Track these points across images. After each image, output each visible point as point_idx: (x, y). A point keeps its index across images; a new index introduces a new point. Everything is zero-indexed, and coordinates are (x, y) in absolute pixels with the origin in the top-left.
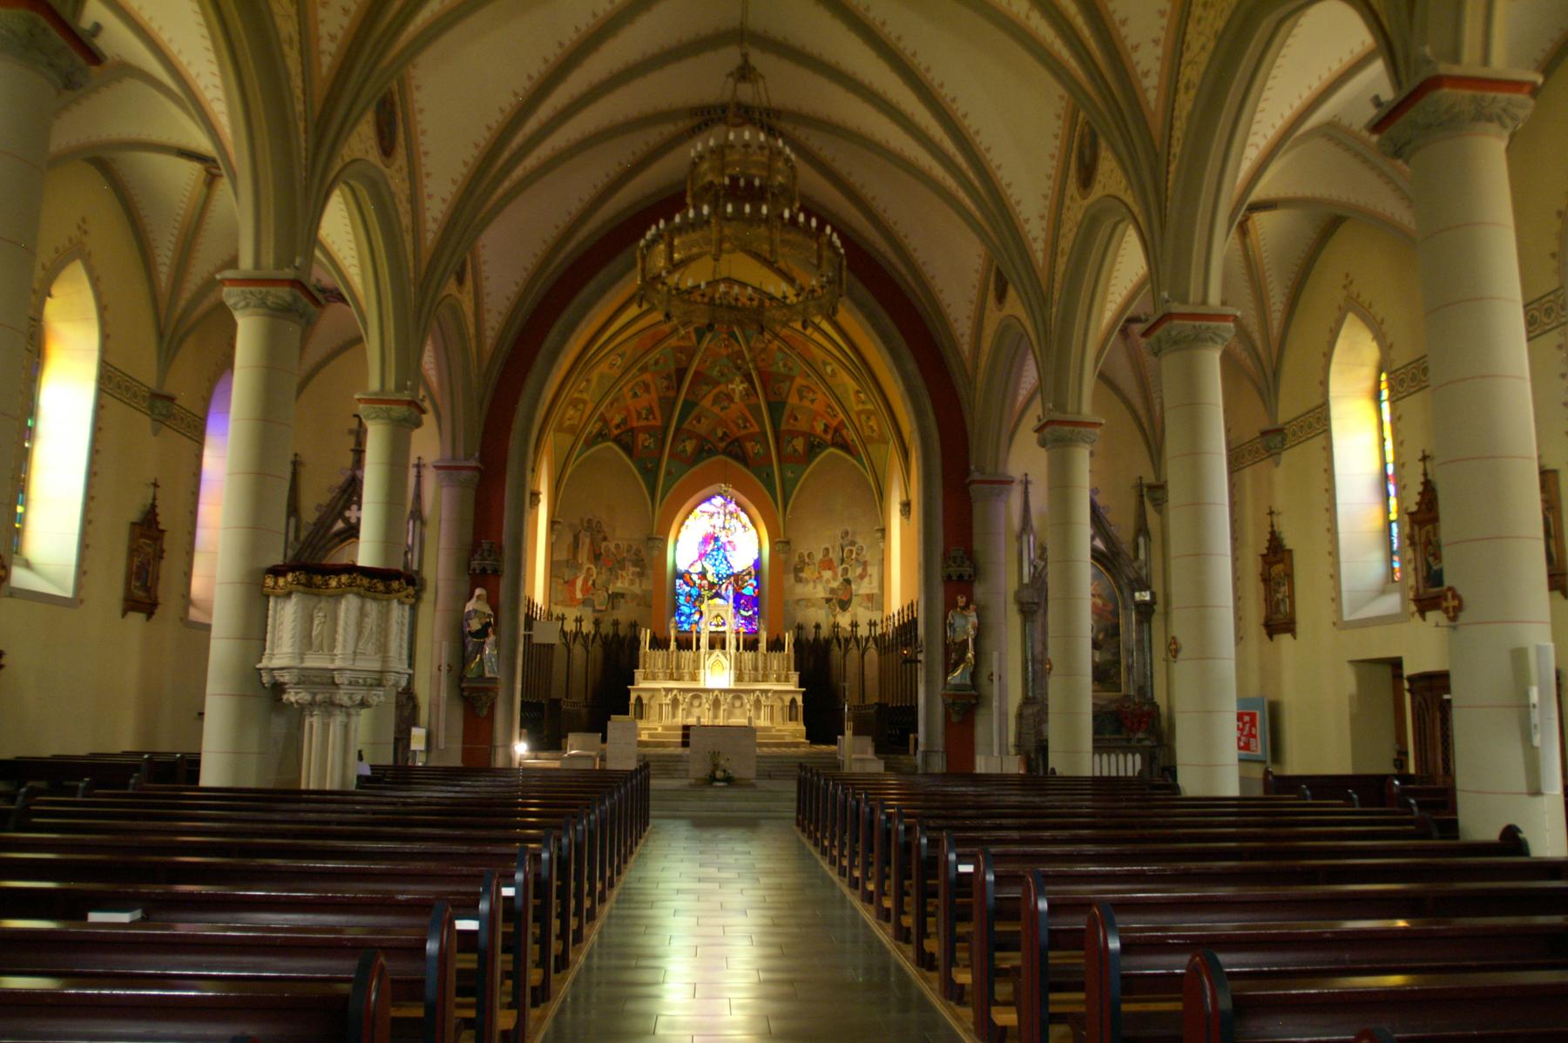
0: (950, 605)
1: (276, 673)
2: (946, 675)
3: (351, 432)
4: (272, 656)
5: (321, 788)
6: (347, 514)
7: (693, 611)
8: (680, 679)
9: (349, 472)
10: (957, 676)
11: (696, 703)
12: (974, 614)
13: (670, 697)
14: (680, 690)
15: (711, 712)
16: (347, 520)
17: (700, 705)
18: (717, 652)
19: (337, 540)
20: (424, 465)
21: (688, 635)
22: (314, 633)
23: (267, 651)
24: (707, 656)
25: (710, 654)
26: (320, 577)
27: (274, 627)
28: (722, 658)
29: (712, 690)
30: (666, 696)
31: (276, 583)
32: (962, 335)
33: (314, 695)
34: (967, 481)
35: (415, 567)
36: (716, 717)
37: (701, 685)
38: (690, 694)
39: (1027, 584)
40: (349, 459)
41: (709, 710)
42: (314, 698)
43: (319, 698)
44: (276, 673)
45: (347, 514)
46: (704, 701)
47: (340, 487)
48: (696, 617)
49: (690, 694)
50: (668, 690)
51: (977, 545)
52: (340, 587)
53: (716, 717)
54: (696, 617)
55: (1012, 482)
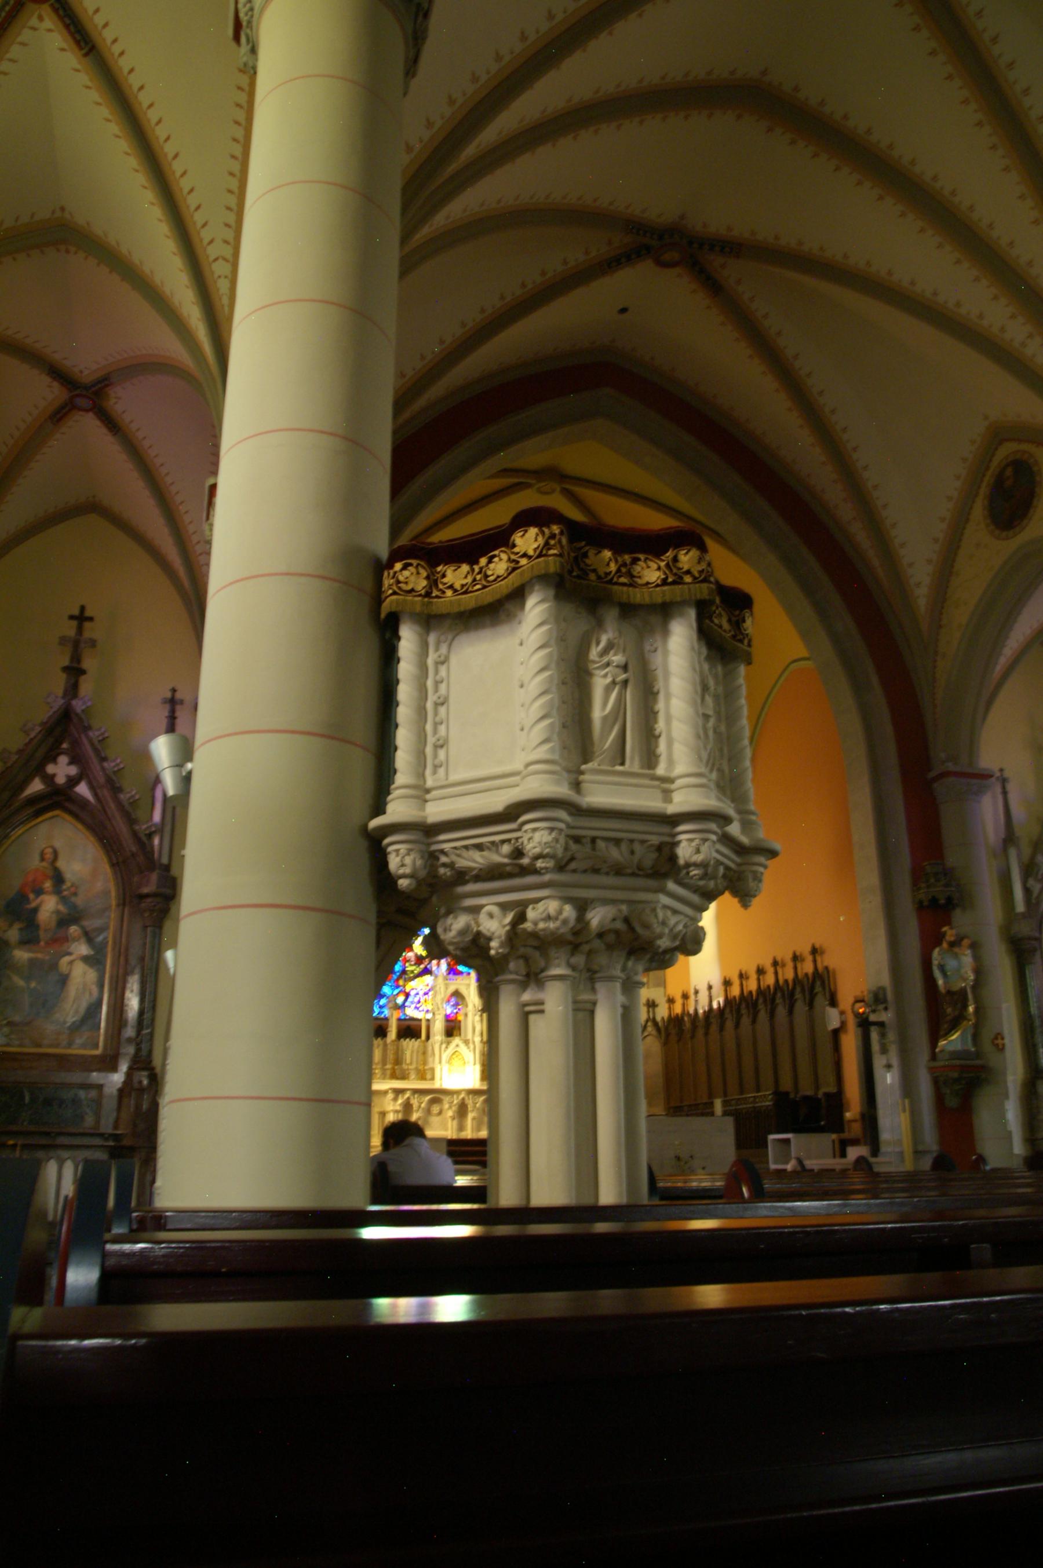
0: (931, 939)
1: (446, 842)
2: (934, 1042)
3: (63, 641)
4: (421, 793)
5: (587, 1201)
6: (50, 769)
7: (396, 992)
8: (404, 1077)
9: (61, 702)
10: (953, 1041)
11: (435, 1109)
12: (968, 952)
13: (400, 1101)
14: (415, 1091)
15: (455, 1122)
16: (49, 779)
17: (440, 1113)
18: (456, 1040)
19: (31, 810)
20: (182, 702)
21: (384, 1022)
22: (598, 713)
23: (402, 778)
24: (444, 1046)
25: (448, 1043)
26: (607, 554)
27: (421, 713)
28: (463, 1048)
29: (458, 1092)
30: (395, 1099)
31: (433, 582)
32: (918, 585)
33: (582, 907)
34: (932, 774)
35: (165, 860)
36: (461, 1128)
37: (437, 1085)
38: (428, 1098)
39: (1023, 914)
40: (59, 683)
41: (453, 1118)
42: (581, 917)
43: (596, 917)
44: (446, 842)
45: (50, 769)
46: (446, 1106)
47: (43, 724)
48: (400, 999)
49: (428, 1098)
50: (398, 1092)
51: (952, 859)
52: (678, 581)
53: (461, 1128)
54: (400, 999)
55: (991, 776)
